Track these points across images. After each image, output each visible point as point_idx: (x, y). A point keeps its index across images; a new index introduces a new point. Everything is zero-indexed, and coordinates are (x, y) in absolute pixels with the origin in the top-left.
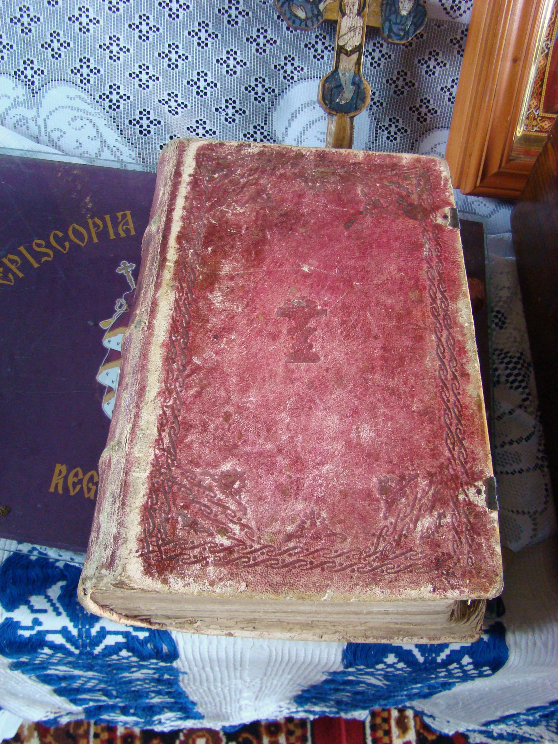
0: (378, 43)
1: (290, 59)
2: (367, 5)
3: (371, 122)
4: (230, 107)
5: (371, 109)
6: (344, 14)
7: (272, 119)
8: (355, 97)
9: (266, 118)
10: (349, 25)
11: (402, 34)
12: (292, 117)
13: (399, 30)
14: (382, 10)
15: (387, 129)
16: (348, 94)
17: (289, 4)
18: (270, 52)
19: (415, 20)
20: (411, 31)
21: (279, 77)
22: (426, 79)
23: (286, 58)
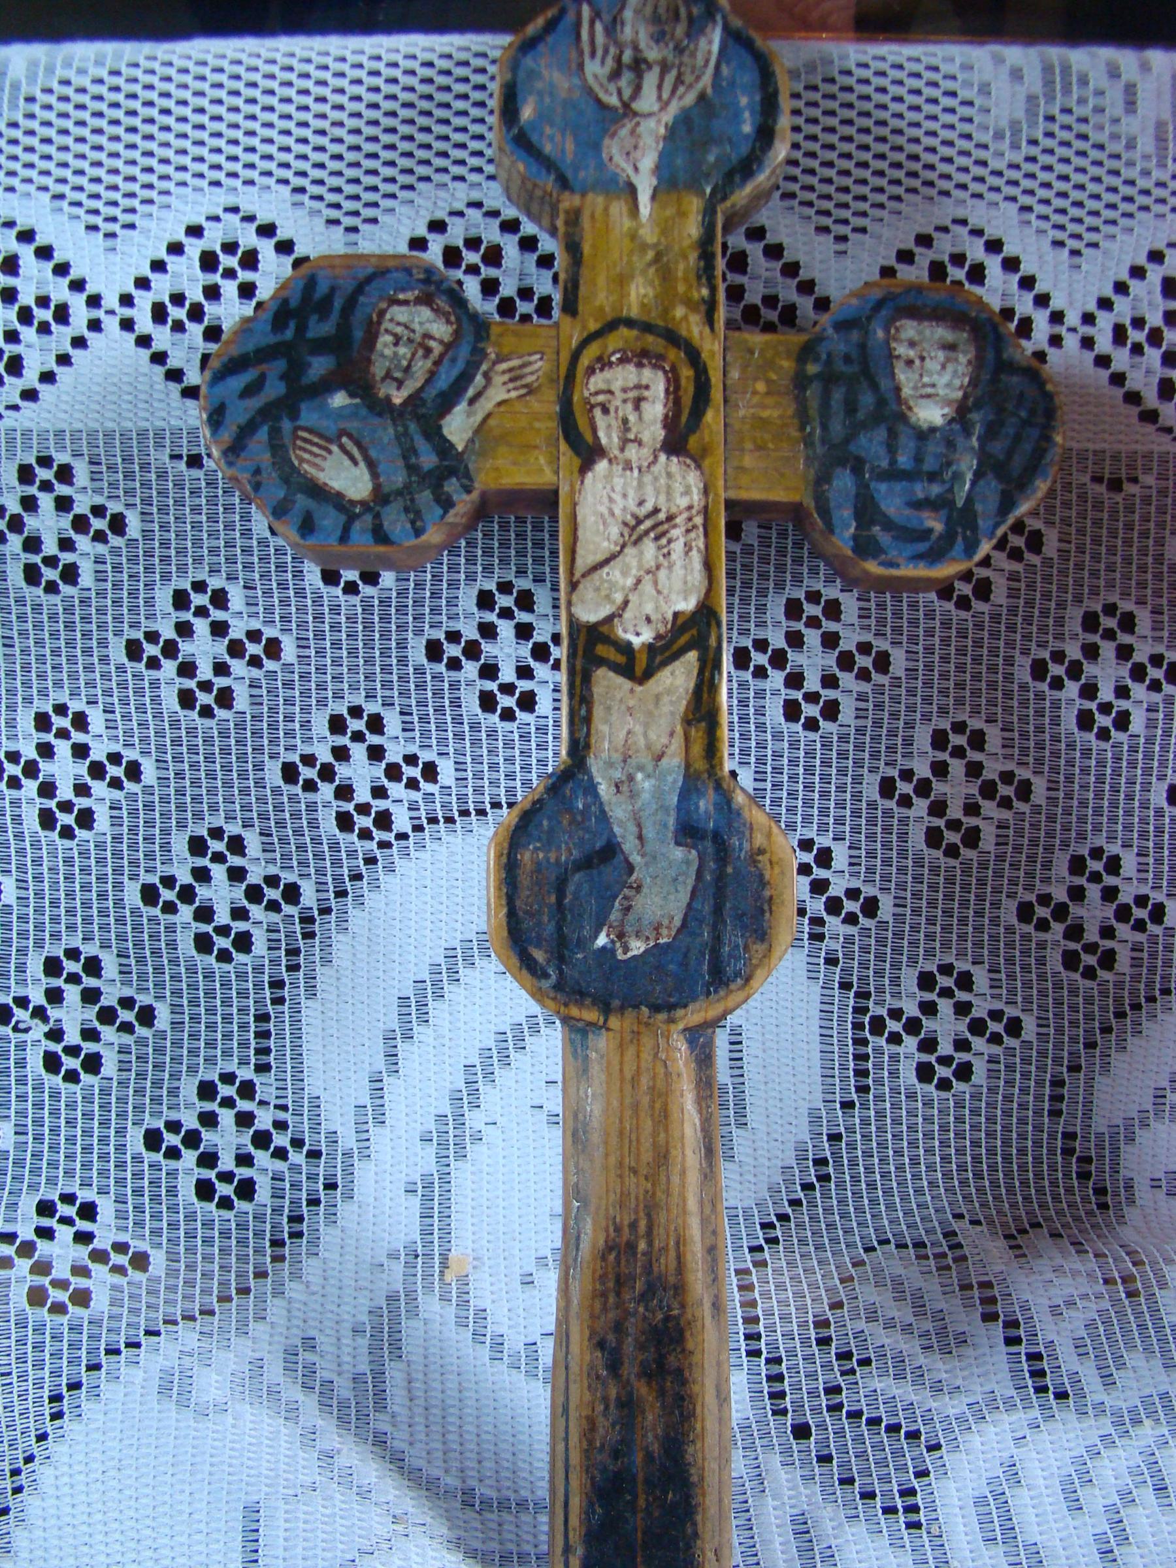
0: (814, 597)
1: (357, 726)
2: (717, 395)
3: (827, 1001)
4: (72, 993)
5: (817, 937)
6: (588, 453)
7: (297, 1035)
8: (706, 908)
9: (264, 1035)
10: (626, 506)
11: (937, 526)
12: (404, 1016)
13: (918, 505)
14: (803, 417)
15: (913, 1026)
16: (661, 895)
17: (275, 432)
18: (255, 701)
19: (998, 448)
20: (986, 507)
21: (314, 824)
22: (1086, 753)
23: (337, 725)
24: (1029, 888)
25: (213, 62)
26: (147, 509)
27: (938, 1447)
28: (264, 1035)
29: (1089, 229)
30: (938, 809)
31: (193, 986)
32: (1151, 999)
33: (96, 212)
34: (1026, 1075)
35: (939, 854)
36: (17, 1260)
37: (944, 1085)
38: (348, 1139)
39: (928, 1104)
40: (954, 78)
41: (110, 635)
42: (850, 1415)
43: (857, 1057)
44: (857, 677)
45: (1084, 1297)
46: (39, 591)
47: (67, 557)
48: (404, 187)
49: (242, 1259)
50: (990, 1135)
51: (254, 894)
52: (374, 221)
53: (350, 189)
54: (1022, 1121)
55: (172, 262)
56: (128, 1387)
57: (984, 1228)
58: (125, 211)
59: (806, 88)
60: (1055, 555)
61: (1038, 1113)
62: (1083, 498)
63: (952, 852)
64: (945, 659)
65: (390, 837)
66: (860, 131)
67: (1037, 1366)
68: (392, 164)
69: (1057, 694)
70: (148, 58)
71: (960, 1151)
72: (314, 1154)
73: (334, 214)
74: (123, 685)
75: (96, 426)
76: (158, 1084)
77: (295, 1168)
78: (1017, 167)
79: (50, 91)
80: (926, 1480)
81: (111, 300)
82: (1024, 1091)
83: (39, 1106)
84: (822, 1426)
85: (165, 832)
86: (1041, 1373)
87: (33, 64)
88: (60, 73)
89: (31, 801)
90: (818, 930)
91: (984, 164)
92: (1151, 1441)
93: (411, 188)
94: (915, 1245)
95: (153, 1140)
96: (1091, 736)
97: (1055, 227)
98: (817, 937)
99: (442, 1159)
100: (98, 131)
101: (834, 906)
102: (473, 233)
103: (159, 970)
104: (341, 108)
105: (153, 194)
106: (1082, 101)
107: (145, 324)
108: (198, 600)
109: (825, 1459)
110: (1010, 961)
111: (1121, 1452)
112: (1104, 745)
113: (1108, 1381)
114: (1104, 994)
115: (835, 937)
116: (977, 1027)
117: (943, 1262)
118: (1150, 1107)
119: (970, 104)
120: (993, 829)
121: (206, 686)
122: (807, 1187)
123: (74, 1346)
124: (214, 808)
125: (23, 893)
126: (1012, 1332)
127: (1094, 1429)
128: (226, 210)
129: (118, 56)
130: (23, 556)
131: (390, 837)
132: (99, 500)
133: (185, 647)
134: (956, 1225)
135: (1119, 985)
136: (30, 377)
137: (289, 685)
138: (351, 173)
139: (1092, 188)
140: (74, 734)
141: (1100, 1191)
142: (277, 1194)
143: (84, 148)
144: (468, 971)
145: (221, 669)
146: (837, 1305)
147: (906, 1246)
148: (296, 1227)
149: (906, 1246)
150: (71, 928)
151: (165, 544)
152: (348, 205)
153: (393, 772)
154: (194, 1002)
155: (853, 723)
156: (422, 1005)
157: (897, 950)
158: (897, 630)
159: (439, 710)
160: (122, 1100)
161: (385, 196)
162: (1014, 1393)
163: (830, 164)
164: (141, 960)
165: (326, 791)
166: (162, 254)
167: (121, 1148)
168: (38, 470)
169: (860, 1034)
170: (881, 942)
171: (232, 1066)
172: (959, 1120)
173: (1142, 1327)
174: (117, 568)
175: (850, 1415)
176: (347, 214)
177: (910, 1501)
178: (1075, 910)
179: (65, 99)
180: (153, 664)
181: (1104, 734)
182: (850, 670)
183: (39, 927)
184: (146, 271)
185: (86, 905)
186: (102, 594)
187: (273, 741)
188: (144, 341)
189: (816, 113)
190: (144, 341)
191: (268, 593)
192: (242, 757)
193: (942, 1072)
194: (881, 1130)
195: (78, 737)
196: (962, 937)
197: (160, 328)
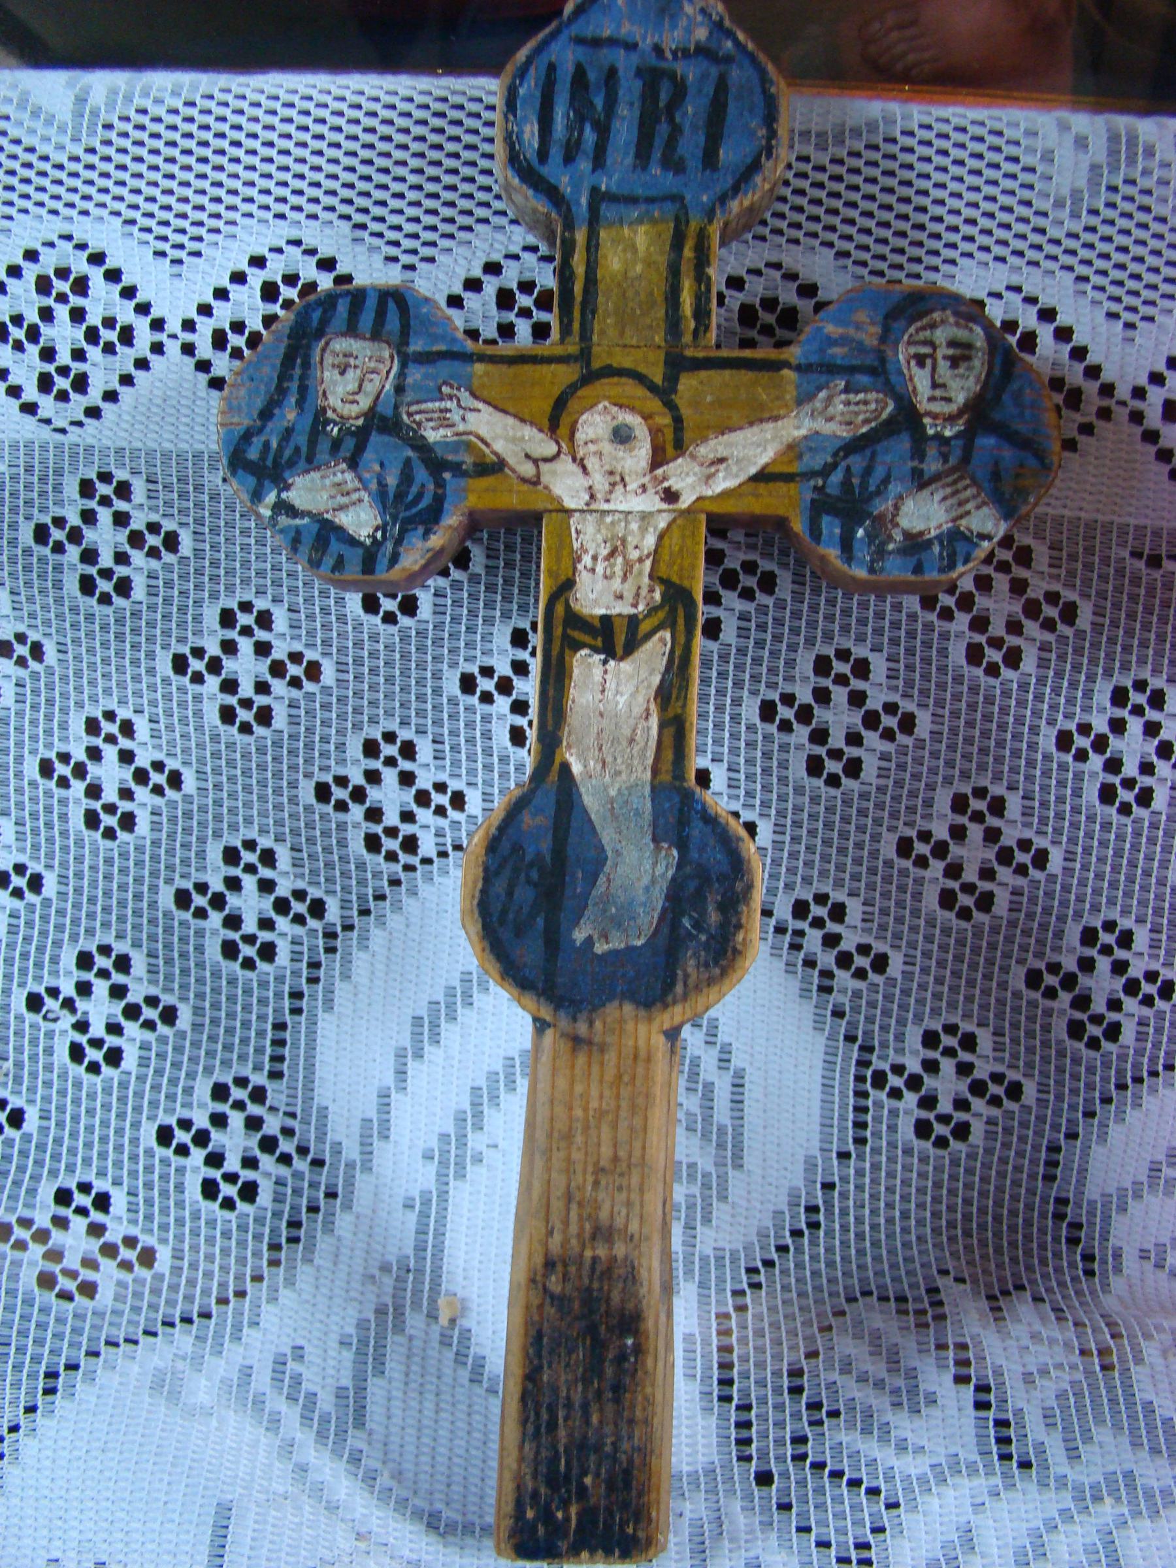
3: (831, 1052)
5: (825, 990)
9: (279, 1043)
12: (417, 1036)
15: (914, 1083)
18: (294, 721)
21: (342, 843)
24: (1039, 955)
25: (285, 97)
26: (200, 529)
27: (896, 1505)
28: (280, 1043)
29: (1145, 303)
30: (953, 871)
31: (216, 991)
32: (1154, 1074)
33: (165, 239)
34: (1022, 1139)
35: (951, 915)
36: (31, 1244)
37: (941, 1142)
38: (352, 1151)
39: (924, 1160)
40: (1017, 143)
41: (158, 649)
42: (814, 1465)
43: (857, 1109)
44: (882, 736)
45: (1059, 1366)
46: (93, 601)
47: (121, 571)
48: (462, 228)
49: (241, 1261)
50: (983, 1194)
51: (282, 906)
52: (431, 260)
53: (409, 228)
54: (1016, 1183)
55: (235, 291)
56: (121, 1378)
57: (968, 1286)
58: (192, 239)
59: (867, 147)
60: (1088, 628)
61: (1032, 1176)
62: (1120, 572)
63: (965, 914)
64: (970, 724)
65: (415, 860)
66: (900, 200)
67: (1004, 1432)
68: (452, 204)
69: (1080, 766)
70: (223, 91)
71: (951, 1209)
72: (318, 1163)
73: (393, 251)
74: (168, 697)
75: (155, 446)
76: (174, 1082)
77: (298, 1175)
78: (1076, 236)
79: (127, 119)
80: (881, 1536)
81: (174, 325)
82: (1020, 1154)
83: (62, 1093)
84: (785, 1475)
85: (202, 840)
86: (1007, 1441)
87: (114, 92)
88: (138, 102)
89: (77, 801)
90: (826, 982)
91: (1043, 231)
92: (1110, 1520)
93: (469, 229)
94: (897, 1299)
95: (164, 1135)
96: (1113, 811)
97: (1111, 298)
98: (825, 990)
99: (442, 1179)
100: (171, 160)
101: (844, 960)
102: (527, 276)
103: (185, 972)
104: (268, 192)
105: (220, 224)
106: (1146, 172)
107: (205, 349)
108: (244, 619)
109: (785, 1507)
110: (1015, 1026)
111: (1078, 1528)
112: (1124, 820)
113: (1073, 1454)
114: (1107, 1065)
115: (843, 991)
116: (978, 1088)
117: (922, 1319)
118: (1144, 1179)
119: (1032, 170)
120: (1007, 895)
121: (247, 703)
122: (797, 1233)
123: (77, 1331)
124: (248, 821)
125: (63, 889)
126: (983, 1397)
127: (1054, 1502)
128: (289, 242)
129: (194, 87)
130: (80, 566)
131: (415, 860)
132: (154, 517)
133: (229, 664)
134: (940, 1282)
135: (1122, 1058)
136: (94, 396)
137: (326, 707)
138: (411, 212)
139: (1151, 261)
140: (121, 739)
141: (1088, 1258)
142: (278, 1199)
143: (156, 176)
144: (483, 996)
145: (262, 688)
146: (812, 1355)
147: (887, 1299)
148: (294, 1233)
149: (887, 1299)
150: (106, 925)
151: (215, 564)
152: (407, 244)
153: (423, 799)
154: (216, 1006)
155: (875, 781)
156: (435, 1026)
157: (904, 1007)
158: (924, 693)
159: (471, 741)
160: (139, 1095)
161: (444, 236)
162: (978, 1458)
163: (886, 225)
164: (169, 962)
165: (357, 811)
166: (225, 282)
167: (135, 1141)
168: (98, 485)
169: (861, 1087)
170: (889, 998)
171: (247, 1071)
172: (953, 1178)
173: (1113, 1401)
174: (169, 584)
175: (814, 1465)
176: (406, 252)
177: (865, 1554)
178: (1083, 980)
179: (141, 127)
180: (198, 678)
181: (1125, 809)
182: (875, 729)
183: (76, 922)
184: (209, 298)
185: (122, 904)
186: (152, 608)
187: (309, 761)
188: (203, 366)
189: (875, 172)
190: (203, 366)
191: (311, 617)
192: (278, 775)
193: (940, 1129)
194: (875, 1181)
195: (124, 743)
196: (969, 999)
197: (219, 354)
